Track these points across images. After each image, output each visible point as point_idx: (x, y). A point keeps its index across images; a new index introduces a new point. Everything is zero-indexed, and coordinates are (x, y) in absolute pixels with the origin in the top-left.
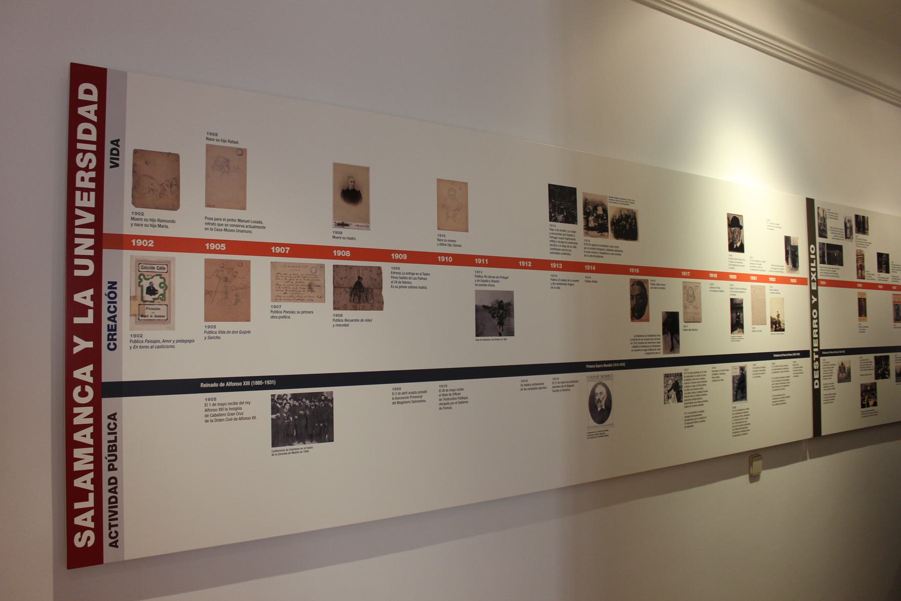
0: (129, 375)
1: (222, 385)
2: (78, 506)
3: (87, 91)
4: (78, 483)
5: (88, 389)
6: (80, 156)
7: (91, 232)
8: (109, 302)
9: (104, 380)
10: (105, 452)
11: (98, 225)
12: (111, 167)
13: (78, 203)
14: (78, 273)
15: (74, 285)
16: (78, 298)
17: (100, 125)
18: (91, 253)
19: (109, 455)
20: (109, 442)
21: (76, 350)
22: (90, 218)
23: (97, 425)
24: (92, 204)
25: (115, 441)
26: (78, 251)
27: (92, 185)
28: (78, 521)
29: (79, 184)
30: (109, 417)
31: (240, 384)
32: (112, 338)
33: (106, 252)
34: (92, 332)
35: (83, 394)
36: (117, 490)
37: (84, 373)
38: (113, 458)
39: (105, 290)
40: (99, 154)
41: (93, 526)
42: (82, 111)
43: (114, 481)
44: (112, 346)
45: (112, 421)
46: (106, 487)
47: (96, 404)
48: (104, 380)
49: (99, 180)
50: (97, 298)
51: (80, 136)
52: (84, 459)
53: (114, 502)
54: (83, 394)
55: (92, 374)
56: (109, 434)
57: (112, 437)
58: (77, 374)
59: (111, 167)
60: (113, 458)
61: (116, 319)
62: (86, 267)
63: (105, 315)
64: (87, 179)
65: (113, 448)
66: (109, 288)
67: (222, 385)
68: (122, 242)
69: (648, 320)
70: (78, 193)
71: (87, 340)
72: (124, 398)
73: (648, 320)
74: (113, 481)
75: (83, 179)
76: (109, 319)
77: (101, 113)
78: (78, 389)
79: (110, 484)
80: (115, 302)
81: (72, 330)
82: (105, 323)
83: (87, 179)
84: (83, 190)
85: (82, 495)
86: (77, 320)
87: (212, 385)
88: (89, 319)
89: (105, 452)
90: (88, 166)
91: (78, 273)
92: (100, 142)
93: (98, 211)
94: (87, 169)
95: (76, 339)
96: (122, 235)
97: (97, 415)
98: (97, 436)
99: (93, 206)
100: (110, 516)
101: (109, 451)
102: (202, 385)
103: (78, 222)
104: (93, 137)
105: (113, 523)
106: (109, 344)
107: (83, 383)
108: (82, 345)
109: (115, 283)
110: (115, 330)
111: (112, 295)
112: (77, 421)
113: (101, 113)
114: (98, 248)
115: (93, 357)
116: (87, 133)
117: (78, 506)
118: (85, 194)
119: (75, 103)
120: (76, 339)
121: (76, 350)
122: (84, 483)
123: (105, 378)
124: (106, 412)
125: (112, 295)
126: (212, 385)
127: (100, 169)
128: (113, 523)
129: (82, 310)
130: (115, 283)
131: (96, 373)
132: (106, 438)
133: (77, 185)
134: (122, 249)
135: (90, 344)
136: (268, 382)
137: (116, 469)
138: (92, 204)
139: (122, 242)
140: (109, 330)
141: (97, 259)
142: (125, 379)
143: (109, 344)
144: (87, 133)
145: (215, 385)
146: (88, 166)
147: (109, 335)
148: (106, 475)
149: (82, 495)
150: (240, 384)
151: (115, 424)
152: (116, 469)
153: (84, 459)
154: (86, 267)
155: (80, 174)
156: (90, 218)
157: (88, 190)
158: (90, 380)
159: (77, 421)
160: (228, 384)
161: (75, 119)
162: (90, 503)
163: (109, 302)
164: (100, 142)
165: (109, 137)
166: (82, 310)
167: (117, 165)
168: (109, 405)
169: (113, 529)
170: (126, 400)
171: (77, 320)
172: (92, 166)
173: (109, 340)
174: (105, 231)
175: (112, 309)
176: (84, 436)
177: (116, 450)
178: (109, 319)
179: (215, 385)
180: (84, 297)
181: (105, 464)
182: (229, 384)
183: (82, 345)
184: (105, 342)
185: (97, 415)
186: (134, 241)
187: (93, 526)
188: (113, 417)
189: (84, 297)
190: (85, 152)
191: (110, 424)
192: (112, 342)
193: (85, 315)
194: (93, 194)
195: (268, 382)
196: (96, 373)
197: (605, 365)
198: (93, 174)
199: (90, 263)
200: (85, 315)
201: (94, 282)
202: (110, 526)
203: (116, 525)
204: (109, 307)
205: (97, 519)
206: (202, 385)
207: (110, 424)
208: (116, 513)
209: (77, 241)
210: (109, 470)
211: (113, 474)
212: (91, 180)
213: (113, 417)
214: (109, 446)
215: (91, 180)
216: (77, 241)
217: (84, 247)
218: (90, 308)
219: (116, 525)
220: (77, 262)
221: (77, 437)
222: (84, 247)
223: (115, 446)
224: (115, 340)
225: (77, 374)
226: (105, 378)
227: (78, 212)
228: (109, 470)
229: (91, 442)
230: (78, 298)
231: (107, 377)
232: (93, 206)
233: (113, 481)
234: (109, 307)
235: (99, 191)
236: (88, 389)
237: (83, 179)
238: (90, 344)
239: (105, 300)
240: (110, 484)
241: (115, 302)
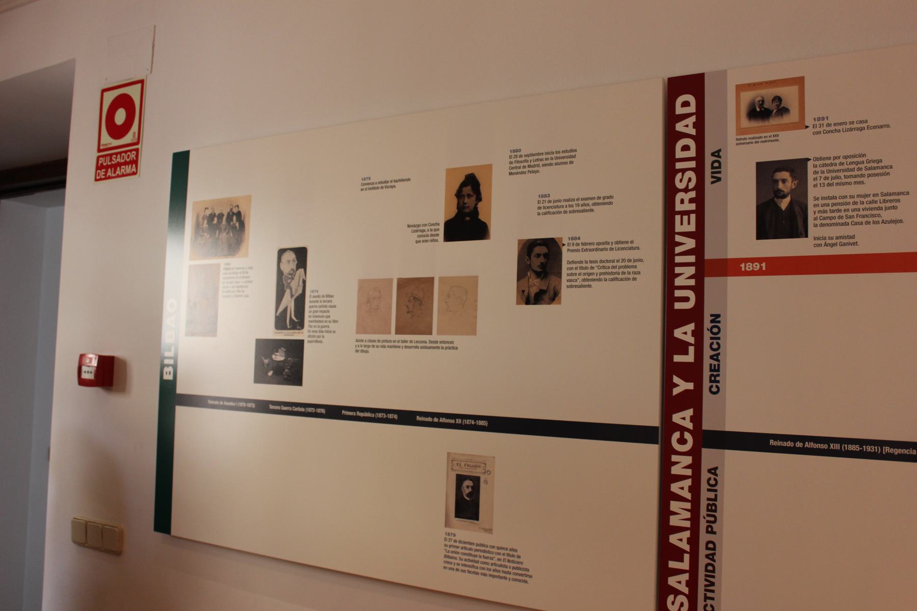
0: (733, 424)
1: (436, 420)
2: (672, 564)
3: (686, 103)
4: (673, 539)
5: (687, 436)
6: (679, 176)
7: (692, 259)
8: (711, 338)
9: (705, 427)
10: (704, 511)
11: (698, 251)
12: (713, 183)
13: (678, 228)
14: (678, 306)
15: (672, 318)
16: (678, 333)
17: (699, 139)
18: (692, 282)
19: (708, 515)
20: (708, 499)
21: (676, 391)
22: (691, 243)
23: (696, 477)
24: (692, 228)
25: (715, 499)
26: (678, 282)
27: (693, 207)
28: (672, 581)
29: (679, 207)
30: (709, 471)
31: (825, 446)
32: (714, 379)
33: (708, 281)
34: (692, 372)
35: (682, 441)
36: (715, 557)
37: (683, 418)
38: (712, 519)
39: (707, 324)
40: (699, 171)
41: (687, 592)
42: (680, 127)
43: (712, 547)
44: (714, 389)
45: (713, 476)
46: (703, 552)
47: (695, 453)
48: (705, 427)
49: (699, 200)
50: (698, 334)
51: (679, 154)
52: (680, 514)
53: (711, 571)
54: (682, 441)
55: (692, 419)
56: (709, 490)
57: (711, 495)
58: (676, 418)
59: (713, 183)
60: (712, 519)
61: (720, 358)
62: (686, 299)
63: (707, 352)
64: (686, 201)
65: (712, 508)
66: (712, 321)
67: (436, 420)
68: (729, 267)
69: (560, 303)
70: (678, 218)
71: (687, 381)
72: (726, 451)
73: (560, 303)
74: (711, 546)
75: (682, 201)
76: (712, 357)
77: (700, 125)
78: (676, 435)
79: (707, 548)
80: (719, 338)
81: (669, 370)
82: (707, 362)
83: (686, 201)
84: (683, 213)
85: (678, 554)
86: (678, 358)
87: (785, 444)
88: (690, 358)
89: (703, 511)
90: (688, 185)
91: (678, 306)
92: (700, 157)
93: (699, 235)
94: (686, 190)
95: (676, 380)
96: (727, 260)
97: (696, 466)
98: (695, 489)
99: (694, 230)
100: (706, 586)
101: (708, 510)
102: (772, 442)
103: (678, 250)
104: (692, 153)
105: (709, 594)
106: (711, 387)
107: (683, 429)
108: (682, 386)
109: (718, 316)
110: (718, 370)
111: (715, 330)
112: (675, 470)
113: (700, 125)
114: (699, 277)
115: (693, 400)
116: (685, 150)
117: (672, 564)
118: (685, 218)
119: (671, 118)
120: (676, 380)
121: (676, 391)
122: (680, 540)
123: (706, 426)
124: (705, 466)
125: (715, 330)
126: (785, 444)
127: (700, 188)
128: (709, 594)
129: (682, 347)
130: (718, 316)
131: (697, 419)
132: (705, 495)
133: (677, 209)
134: (726, 275)
135: (690, 386)
136: (390, 416)
137: (715, 533)
138: (692, 228)
139: (729, 267)
140: (711, 370)
141: (699, 290)
142: (729, 428)
143: (711, 387)
144: (685, 150)
145: (789, 444)
146: (688, 185)
147: (711, 376)
148: (704, 537)
149: (678, 554)
150: (825, 446)
151: (715, 479)
152: (715, 533)
153: (680, 514)
154: (686, 299)
155: (679, 196)
156: (691, 243)
157: (688, 213)
158: (690, 426)
159: (675, 470)
160: (807, 445)
161: (671, 137)
162: (685, 565)
163: (711, 338)
164: (700, 157)
165: (709, 149)
166: (682, 347)
167: (719, 179)
168: (709, 456)
169: (709, 602)
170: (729, 454)
171: (678, 358)
172: (692, 185)
173: (711, 381)
174: (707, 257)
175: (715, 346)
176: (681, 488)
177: (715, 511)
178: (712, 357)
179: (789, 444)
180: (684, 333)
181: (703, 525)
182: (443, 420)
183: (682, 386)
184: (706, 384)
185: (696, 466)
186: (743, 265)
187: (687, 592)
188: (713, 471)
189: (684, 333)
190: (683, 171)
191: (709, 479)
192: (714, 384)
193: (686, 353)
194: (693, 217)
195: (390, 416)
196: (697, 419)
197: (359, 414)
198: (693, 194)
199: (691, 294)
200: (686, 353)
201: (695, 315)
202: (706, 598)
203: (713, 599)
204: (712, 344)
205: (692, 584)
206: (772, 442)
207: (709, 479)
208: (713, 584)
209: (678, 270)
210: (707, 532)
211: (711, 537)
212: (691, 201)
213: (713, 471)
214: (709, 505)
215: (691, 201)
216: (678, 270)
217: (685, 276)
218: (691, 345)
219: (713, 599)
220: (678, 293)
221: (675, 487)
222: (685, 276)
223: (715, 505)
224: (718, 382)
225: (676, 418)
226: (706, 426)
227: (678, 238)
228: (707, 532)
229: (688, 496)
230: (678, 333)
231: (708, 424)
232: (694, 230)
233: (711, 546)
234: (712, 344)
235: (700, 213)
236: (687, 436)
237: (682, 201)
238: (690, 386)
239: (707, 335)
240: (707, 548)
241: (719, 338)
